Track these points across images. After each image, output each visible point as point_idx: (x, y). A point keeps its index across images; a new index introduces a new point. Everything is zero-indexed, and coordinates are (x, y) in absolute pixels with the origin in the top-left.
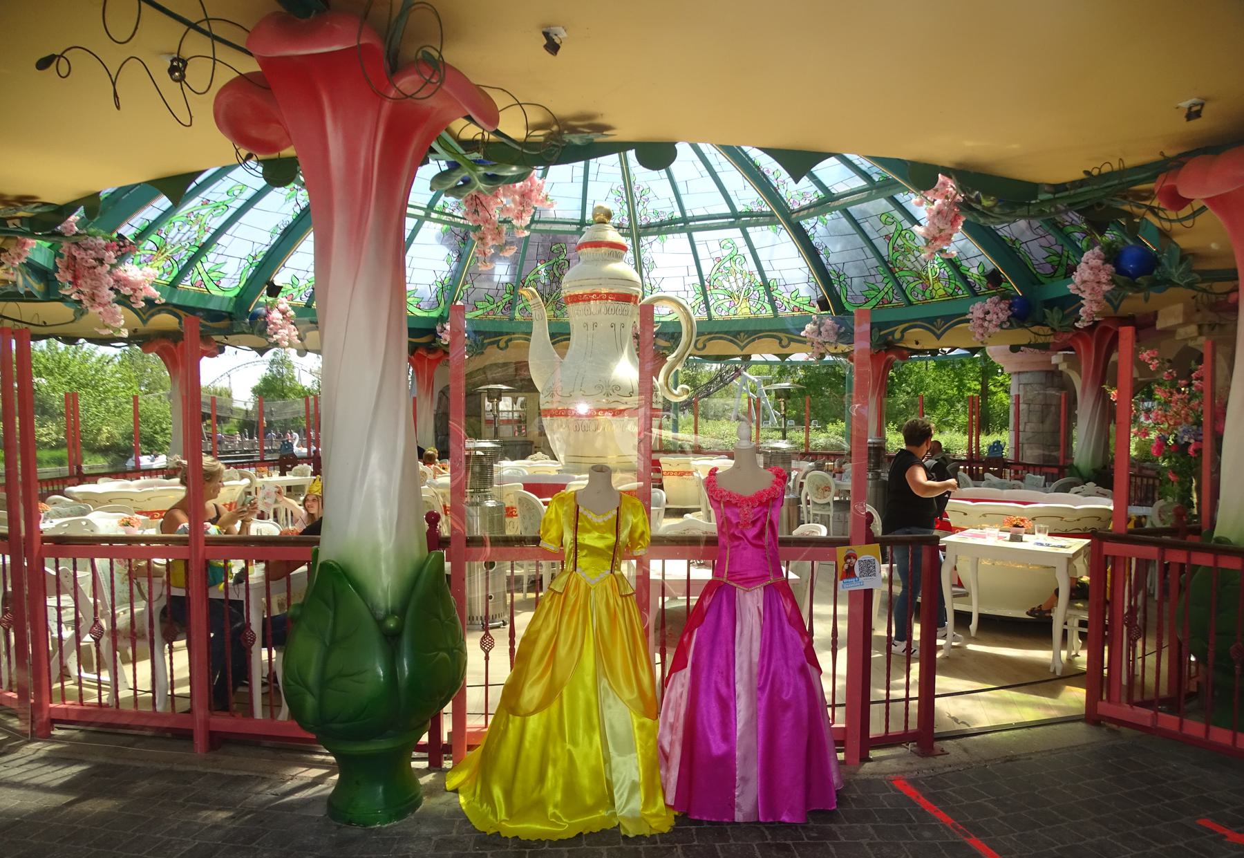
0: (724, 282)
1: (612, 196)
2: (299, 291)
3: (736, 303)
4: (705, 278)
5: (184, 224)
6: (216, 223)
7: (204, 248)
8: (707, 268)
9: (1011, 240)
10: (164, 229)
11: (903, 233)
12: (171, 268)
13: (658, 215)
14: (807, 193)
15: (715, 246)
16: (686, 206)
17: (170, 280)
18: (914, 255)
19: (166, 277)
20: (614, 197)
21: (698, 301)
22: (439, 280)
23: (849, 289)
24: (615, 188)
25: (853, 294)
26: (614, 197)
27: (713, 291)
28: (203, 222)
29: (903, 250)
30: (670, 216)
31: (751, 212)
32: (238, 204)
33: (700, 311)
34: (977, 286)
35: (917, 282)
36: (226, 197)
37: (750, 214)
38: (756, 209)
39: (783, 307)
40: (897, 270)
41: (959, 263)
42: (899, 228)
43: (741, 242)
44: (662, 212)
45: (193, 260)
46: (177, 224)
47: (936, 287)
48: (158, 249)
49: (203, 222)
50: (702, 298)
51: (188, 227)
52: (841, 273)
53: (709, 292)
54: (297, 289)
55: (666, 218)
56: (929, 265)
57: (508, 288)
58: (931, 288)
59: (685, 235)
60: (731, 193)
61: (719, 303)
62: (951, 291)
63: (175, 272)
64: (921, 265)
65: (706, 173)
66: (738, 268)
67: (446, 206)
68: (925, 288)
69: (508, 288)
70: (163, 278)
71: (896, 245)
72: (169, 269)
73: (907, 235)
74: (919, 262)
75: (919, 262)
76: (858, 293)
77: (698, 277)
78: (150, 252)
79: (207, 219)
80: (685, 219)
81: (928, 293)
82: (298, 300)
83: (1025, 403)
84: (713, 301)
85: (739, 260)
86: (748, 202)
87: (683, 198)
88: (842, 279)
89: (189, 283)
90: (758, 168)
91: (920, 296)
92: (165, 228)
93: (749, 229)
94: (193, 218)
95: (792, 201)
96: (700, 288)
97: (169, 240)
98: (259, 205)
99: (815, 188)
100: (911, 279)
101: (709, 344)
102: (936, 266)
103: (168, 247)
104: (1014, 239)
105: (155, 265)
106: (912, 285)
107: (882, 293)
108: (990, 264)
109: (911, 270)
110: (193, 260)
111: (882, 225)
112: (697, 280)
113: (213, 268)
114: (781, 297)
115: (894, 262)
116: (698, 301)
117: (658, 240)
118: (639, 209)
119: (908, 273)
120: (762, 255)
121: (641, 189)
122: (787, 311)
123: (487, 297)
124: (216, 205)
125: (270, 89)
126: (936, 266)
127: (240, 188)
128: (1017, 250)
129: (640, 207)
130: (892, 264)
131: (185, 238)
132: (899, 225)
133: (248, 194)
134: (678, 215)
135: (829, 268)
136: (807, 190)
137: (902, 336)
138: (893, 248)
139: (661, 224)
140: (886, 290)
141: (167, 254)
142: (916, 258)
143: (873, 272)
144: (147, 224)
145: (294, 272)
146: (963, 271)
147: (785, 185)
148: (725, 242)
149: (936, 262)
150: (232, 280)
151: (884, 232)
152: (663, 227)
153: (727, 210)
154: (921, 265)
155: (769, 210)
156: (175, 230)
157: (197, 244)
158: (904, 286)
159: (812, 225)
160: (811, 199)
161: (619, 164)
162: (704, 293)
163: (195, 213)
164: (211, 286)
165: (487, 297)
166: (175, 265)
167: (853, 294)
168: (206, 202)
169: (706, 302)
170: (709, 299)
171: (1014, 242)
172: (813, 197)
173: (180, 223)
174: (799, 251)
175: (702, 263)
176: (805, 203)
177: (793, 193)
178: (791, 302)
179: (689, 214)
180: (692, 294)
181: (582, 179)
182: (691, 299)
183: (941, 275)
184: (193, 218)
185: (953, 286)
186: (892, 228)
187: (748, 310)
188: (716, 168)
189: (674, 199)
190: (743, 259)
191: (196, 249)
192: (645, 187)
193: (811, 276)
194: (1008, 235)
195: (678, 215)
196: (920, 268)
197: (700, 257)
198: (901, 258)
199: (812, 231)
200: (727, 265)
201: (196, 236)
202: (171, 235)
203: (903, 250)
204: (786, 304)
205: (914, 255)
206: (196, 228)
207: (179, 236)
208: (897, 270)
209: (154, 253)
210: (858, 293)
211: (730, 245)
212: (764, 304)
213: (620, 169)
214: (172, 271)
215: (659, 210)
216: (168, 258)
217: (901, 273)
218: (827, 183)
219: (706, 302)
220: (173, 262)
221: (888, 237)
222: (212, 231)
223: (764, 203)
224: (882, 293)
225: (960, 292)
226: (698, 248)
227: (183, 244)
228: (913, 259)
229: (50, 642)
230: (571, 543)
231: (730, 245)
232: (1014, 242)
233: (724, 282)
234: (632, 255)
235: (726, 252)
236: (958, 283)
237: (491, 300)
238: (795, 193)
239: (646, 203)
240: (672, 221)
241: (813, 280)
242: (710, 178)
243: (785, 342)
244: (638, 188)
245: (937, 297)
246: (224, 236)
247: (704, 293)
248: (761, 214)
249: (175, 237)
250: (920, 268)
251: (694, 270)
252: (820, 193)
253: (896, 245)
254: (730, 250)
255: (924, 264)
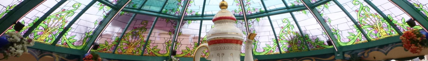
2: (109, 47)
4: (277, 36)
5: (55, 19)
6: (70, 19)
7: (66, 30)
8: (278, 32)
9: (418, 5)
10: (46, 21)
11: (364, 8)
12: (52, 37)
13: (254, 10)
15: (280, 22)
16: (266, 6)
17: (52, 42)
18: (370, 18)
19: (50, 41)
20: (236, 3)
22: (167, 42)
23: (341, 36)
26: (236, 3)
27: (282, 41)
28: (64, 19)
29: (364, 16)
30: (260, 10)
31: (294, 6)
32: (78, 11)
34: (402, 29)
35: (372, 30)
36: (72, 8)
37: (294, 7)
38: (296, 4)
39: (312, 46)
40: (362, 25)
41: (392, 19)
42: (362, 6)
43: (291, 19)
44: (257, 9)
45: (62, 34)
46: (52, 19)
47: (382, 31)
48: (45, 29)
49: (64, 19)
50: (277, 44)
51: (57, 21)
52: (337, 29)
53: (279, 42)
54: (108, 46)
55: (258, 11)
56: (377, 22)
57: (195, 44)
58: (379, 32)
59: (267, 18)
61: (284, 46)
62: (389, 33)
63: (54, 39)
64: (374, 22)
66: (291, 30)
67: (167, 11)
68: (376, 32)
69: (195, 44)
70: (49, 42)
71: (361, 14)
72: (51, 38)
73: (366, 9)
76: (345, 37)
77: (274, 36)
78: (42, 31)
79: (65, 17)
80: (266, 11)
81: (378, 35)
82: (109, 50)
84: (282, 45)
88: (337, 32)
89: (60, 44)
91: (374, 36)
92: (46, 20)
94: (59, 17)
96: (275, 40)
97: (49, 26)
98: (87, 12)
100: (369, 29)
102: (381, 22)
103: (50, 29)
106: (370, 32)
107: (356, 37)
108: (408, 18)
110: (62, 34)
111: (354, 6)
112: (274, 37)
114: (311, 42)
115: (360, 22)
116: (275, 46)
118: (246, 8)
119: (368, 26)
120: (300, 24)
122: (314, 47)
124: (69, 11)
125: (194, 39)
126: (381, 22)
127: (78, 4)
128: (420, 9)
129: (247, 7)
130: (360, 23)
131: (56, 25)
134: (263, 9)
135: (331, 27)
137: (368, 55)
138: (360, 16)
140: (358, 35)
141: (49, 31)
142: (371, 19)
143: (351, 28)
144: (38, 19)
146: (394, 23)
148: (285, 20)
149: (381, 20)
151: (355, 9)
152: (259, 15)
153: (283, 6)
154: (374, 22)
155: (302, 4)
156: (51, 22)
157: (63, 28)
159: (322, 9)
163: (59, 15)
164: (70, 45)
166: (54, 36)
168: (64, 10)
169: (278, 46)
170: (280, 45)
171: (419, 6)
173: (53, 19)
174: (317, 21)
175: (275, 30)
178: (315, 43)
179: (268, 9)
180: (272, 43)
183: (384, 26)
184: (59, 17)
185: (390, 30)
186: (358, 7)
190: (293, 27)
191: (62, 30)
193: (323, 32)
194: (416, 3)
195: (263, 9)
196: (373, 23)
197: (274, 27)
199: (322, 12)
200: (286, 29)
201: (61, 24)
202: (50, 24)
203: (364, 16)
204: (313, 44)
205: (370, 18)
208: (362, 25)
209: (43, 31)
210: (345, 37)
211: (287, 21)
212: (304, 45)
215: (255, 8)
216: (50, 33)
217: (364, 27)
219: (278, 46)
220: (53, 35)
221: (357, 11)
222: (68, 22)
224: (356, 37)
227: (56, 27)
228: (369, 20)
231: (287, 21)
232: (419, 6)
234: (245, 28)
235: (285, 24)
239: (249, 5)
240: (261, 13)
241: (325, 33)
245: (382, 36)
246: (74, 24)
248: (299, 6)
249: (52, 24)
250: (373, 23)
251: (273, 33)
254: (287, 23)
255: (375, 21)
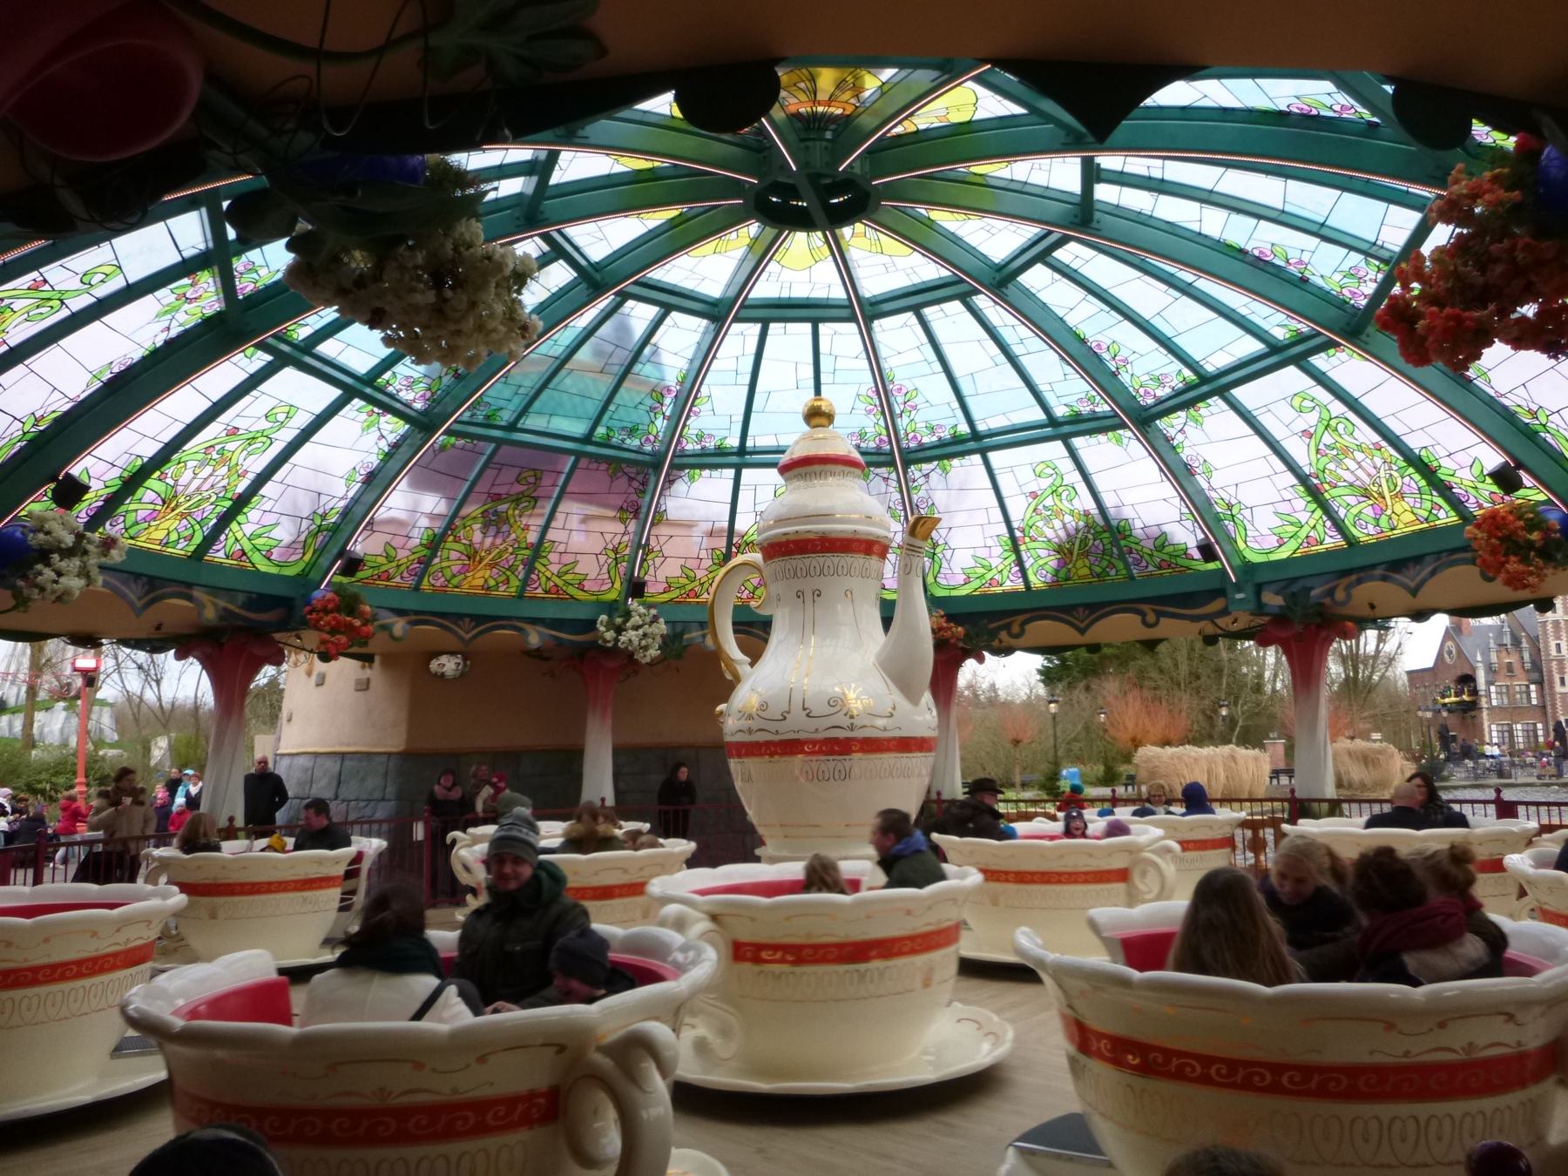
0: (1045, 529)
1: (861, 406)
2: (398, 566)
3: (1068, 561)
4: (1015, 525)
5: (203, 464)
6: (257, 464)
7: (241, 502)
8: (1017, 510)
9: (1530, 411)
11: (1333, 423)
12: (191, 531)
13: (932, 430)
14: (1166, 375)
15: (1026, 474)
16: (976, 414)
17: (192, 548)
18: (1354, 459)
20: (864, 406)
21: (1006, 563)
22: (610, 547)
23: (1249, 526)
24: (863, 391)
25: (1256, 534)
26: (864, 406)
31: (1078, 414)
33: (1012, 578)
34: (1472, 500)
35: (1364, 505)
37: (1077, 419)
38: (1085, 409)
39: (1144, 564)
40: (1327, 487)
41: (1435, 464)
42: (1326, 415)
43: (1067, 465)
44: (940, 426)
45: (226, 519)
47: (1398, 508)
48: (164, 502)
51: (209, 470)
52: (1234, 501)
53: (1023, 548)
54: (394, 564)
56: (1382, 474)
57: (715, 557)
58: (1389, 512)
60: (1043, 388)
61: (1041, 562)
62: (1425, 514)
63: (198, 539)
64: (1369, 475)
65: (1002, 358)
66: (1066, 506)
68: (1379, 512)
69: (715, 557)
70: (179, 546)
72: (187, 533)
73: (1341, 427)
74: (1364, 470)
75: (1364, 470)
77: (1004, 525)
78: (152, 506)
80: (976, 435)
83: (598, 353)
84: (1032, 560)
85: (1067, 492)
86: (1071, 400)
87: (970, 402)
88: (1235, 511)
89: (221, 554)
90: (1083, 341)
91: (1370, 527)
92: (170, 469)
93: (1077, 442)
94: (215, 456)
95: (1142, 391)
96: (1009, 542)
97: (180, 489)
99: (1178, 365)
100: (1352, 500)
101: (1028, 627)
102: (1396, 474)
103: (182, 500)
104: (1535, 408)
105: (161, 526)
106: (1354, 511)
107: (1306, 530)
108: (1493, 459)
109: (1351, 485)
110: (226, 519)
111: (1296, 414)
112: (1003, 529)
113: (259, 532)
114: (1140, 548)
115: (1321, 475)
116: (1006, 563)
117: (938, 470)
118: (902, 423)
119: (1347, 491)
120: (1100, 482)
121: (904, 391)
122: (1151, 568)
123: (685, 570)
124: (251, 435)
126: (1396, 474)
127: (287, 409)
128: (1539, 428)
130: (1317, 477)
132: (1324, 411)
133: (302, 420)
134: (964, 429)
135: (1213, 494)
136: (1164, 371)
137: (1349, 596)
138: (1318, 451)
139: (942, 444)
140: (1312, 523)
141: (180, 509)
142: (1359, 463)
143: (1287, 496)
144: (139, 462)
145: (388, 538)
146: (1443, 477)
147: (1129, 366)
148: (1043, 466)
149: (1395, 467)
150: (291, 551)
151: (1301, 425)
152: (949, 449)
153: (1038, 415)
154: (1369, 475)
155: (1107, 408)
156: (188, 474)
157: (229, 495)
158: (1342, 513)
159: (1179, 428)
160: (1173, 384)
161: (864, 355)
162: (1016, 548)
163: (218, 447)
164: (257, 558)
165: (685, 570)
166: (197, 527)
167: (1256, 534)
168: (233, 432)
169: (1020, 562)
170: (1025, 558)
172: (1176, 382)
173: (195, 463)
175: (1008, 502)
176: (1163, 392)
177: (1144, 378)
178: (1155, 553)
179: (981, 427)
180: (997, 551)
181: (811, 383)
182: (999, 557)
184: (215, 456)
185: (1428, 505)
187: (1087, 572)
188: (1017, 350)
189: (956, 405)
191: (228, 504)
192: (911, 388)
193: (1185, 510)
194: (1524, 404)
195: (964, 429)
196: (1367, 480)
197: (1005, 492)
198: (1332, 466)
199: (1180, 437)
200: (1049, 502)
201: (225, 482)
202: (183, 480)
205: (1354, 459)
206: (223, 470)
207: (196, 483)
208: (1327, 487)
209: (159, 508)
211: (1050, 471)
212: (1113, 560)
213: (866, 362)
214: (192, 536)
215: (934, 423)
216: (183, 516)
217: (1334, 492)
218: (1196, 354)
219: (1020, 562)
220: (193, 522)
221: (1307, 434)
222: (251, 476)
223: (1098, 398)
224: (1306, 530)
225: (1442, 514)
226: (1000, 479)
227: (205, 494)
229: (1559, 704)
230: (455, 1091)
231: (1050, 471)
233: (1045, 529)
235: (1045, 483)
236: (1435, 499)
237: (691, 574)
238: (1147, 377)
239: (913, 413)
240: (957, 440)
241: (1190, 517)
242: (1008, 365)
243: (1151, 618)
244: (900, 390)
245: (1401, 525)
247: (1016, 548)
248: (1094, 417)
250: (1367, 480)
251: (997, 514)
252: (1188, 373)
253: (1322, 446)
254: (1050, 480)
